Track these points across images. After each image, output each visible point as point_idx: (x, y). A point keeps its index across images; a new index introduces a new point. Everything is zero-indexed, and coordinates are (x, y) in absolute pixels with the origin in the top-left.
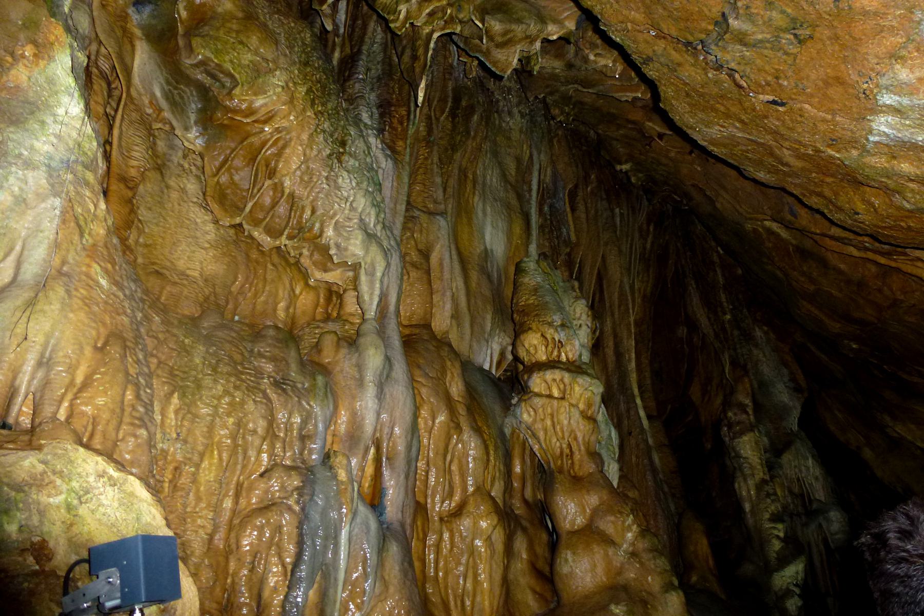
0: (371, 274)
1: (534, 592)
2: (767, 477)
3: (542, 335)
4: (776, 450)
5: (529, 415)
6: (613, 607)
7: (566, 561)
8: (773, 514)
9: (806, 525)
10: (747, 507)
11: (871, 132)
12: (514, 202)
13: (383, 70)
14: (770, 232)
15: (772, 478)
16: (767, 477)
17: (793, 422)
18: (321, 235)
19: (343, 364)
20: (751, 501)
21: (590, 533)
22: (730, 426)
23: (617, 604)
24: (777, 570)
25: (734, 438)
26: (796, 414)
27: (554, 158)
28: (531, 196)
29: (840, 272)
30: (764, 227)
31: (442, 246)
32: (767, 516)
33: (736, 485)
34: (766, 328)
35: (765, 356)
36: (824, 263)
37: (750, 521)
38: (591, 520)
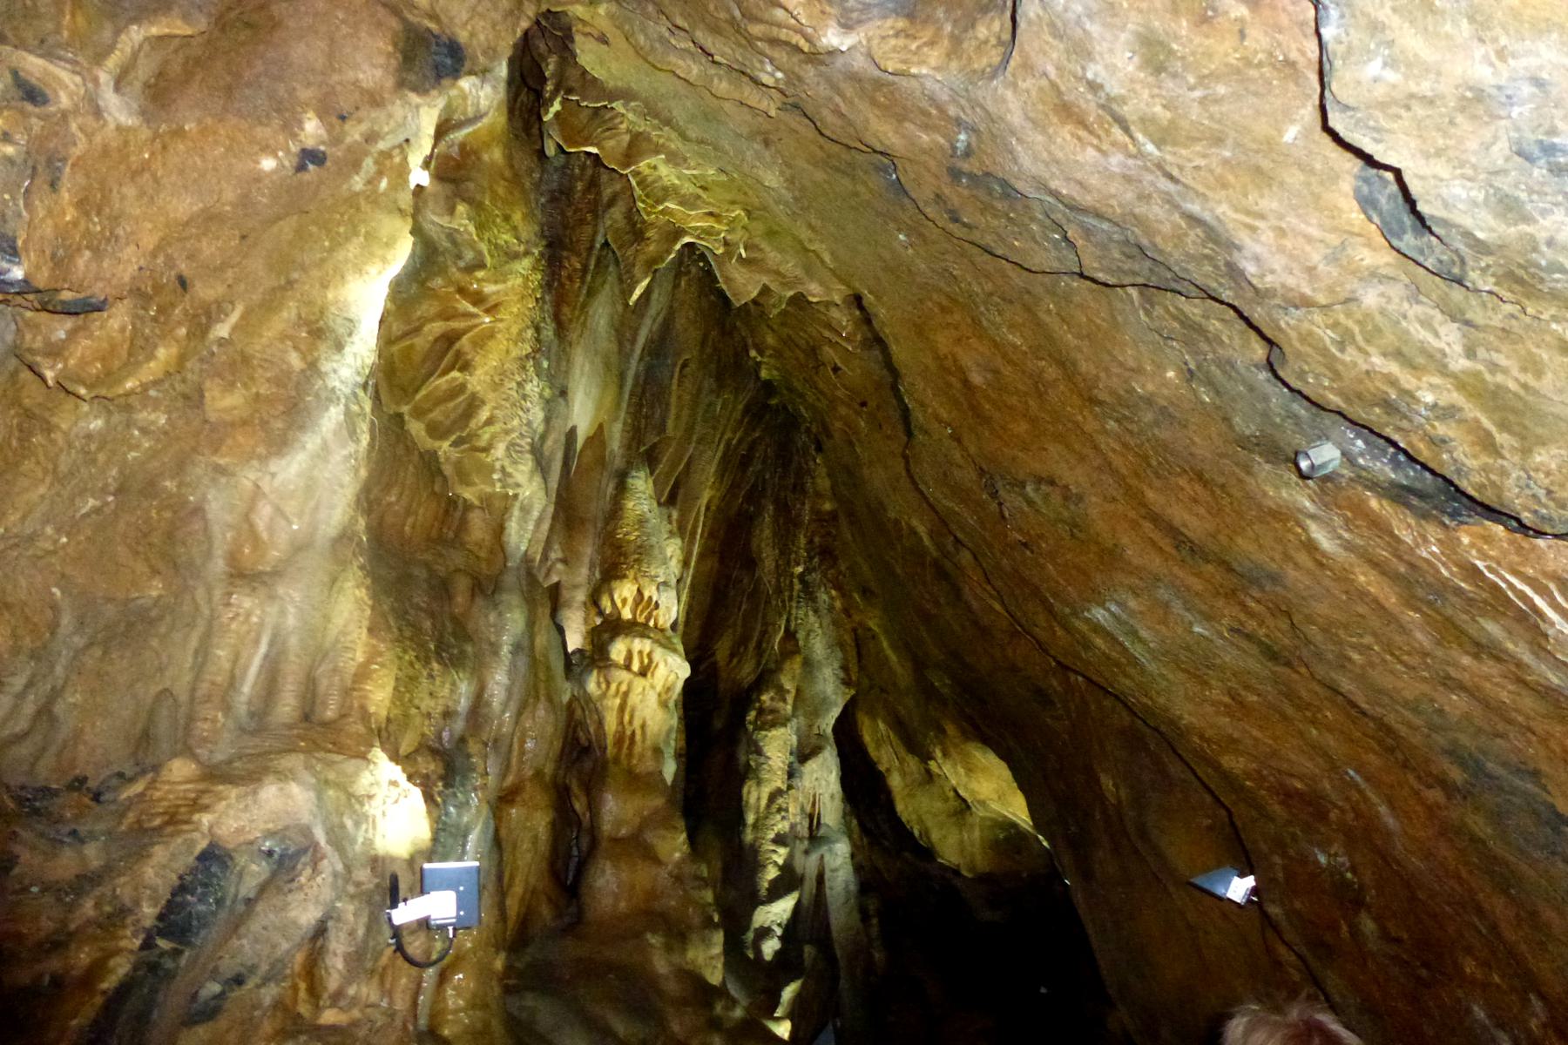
0: (526, 510)
1: (550, 900)
2: (784, 787)
3: (639, 590)
4: (804, 753)
5: (599, 684)
6: (649, 936)
7: (603, 871)
8: (778, 835)
9: (807, 852)
10: (751, 818)
11: (1089, 610)
12: (614, 359)
13: (561, 184)
14: (913, 532)
15: (790, 787)
16: (784, 787)
17: (828, 722)
18: (486, 450)
19: (484, 620)
20: (757, 812)
21: (636, 847)
22: (761, 711)
23: (654, 932)
24: (763, 903)
25: (761, 728)
26: (835, 712)
27: (676, 305)
28: (632, 350)
29: (969, 609)
30: (908, 525)
31: (556, 442)
32: (771, 835)
33: (745, 790)
34: (834, 592)
35: (821, 626)
36: (957, 593)
37: (749, 836)
38: (640, 829)
